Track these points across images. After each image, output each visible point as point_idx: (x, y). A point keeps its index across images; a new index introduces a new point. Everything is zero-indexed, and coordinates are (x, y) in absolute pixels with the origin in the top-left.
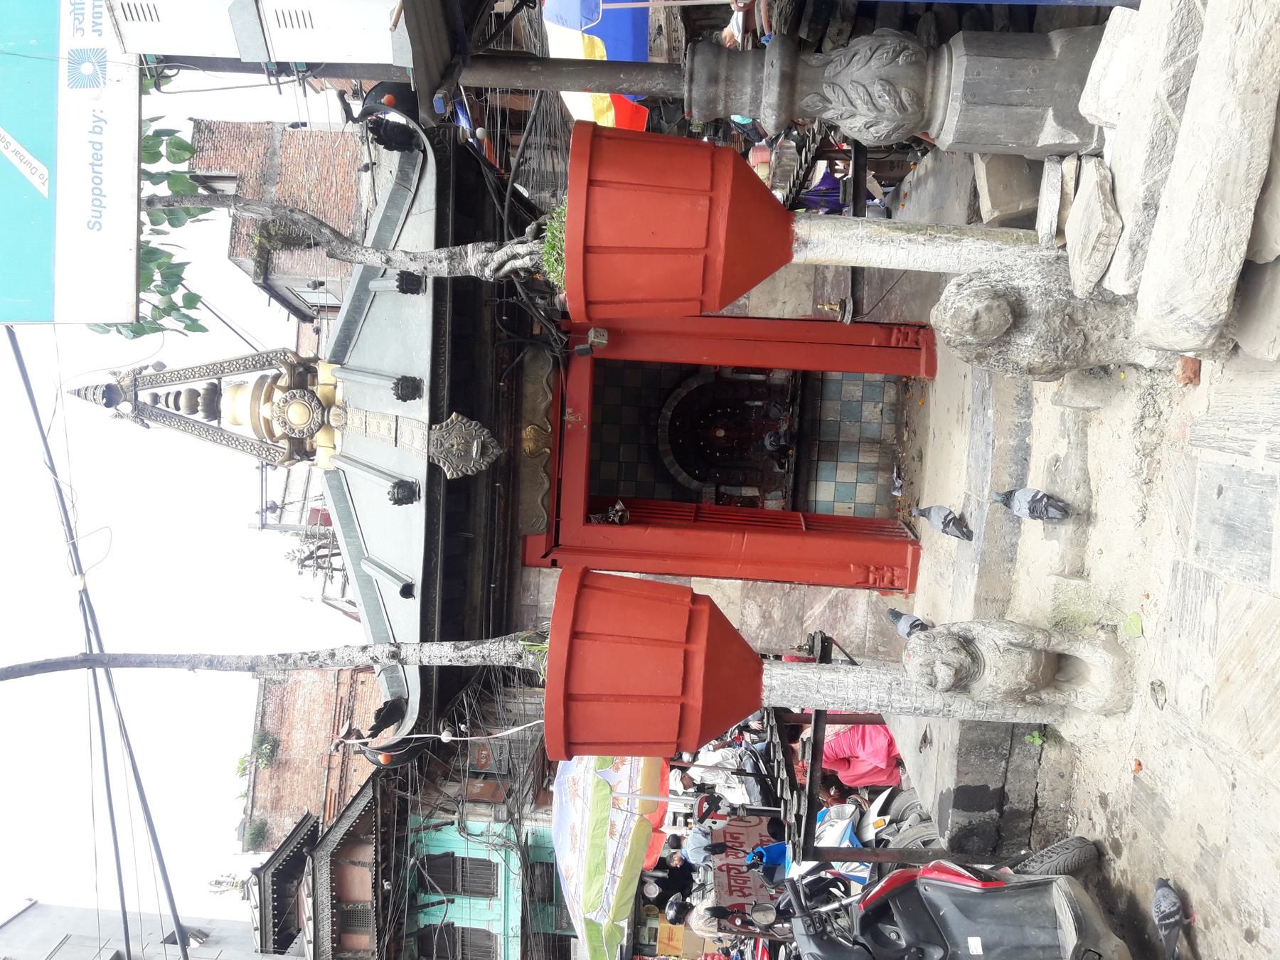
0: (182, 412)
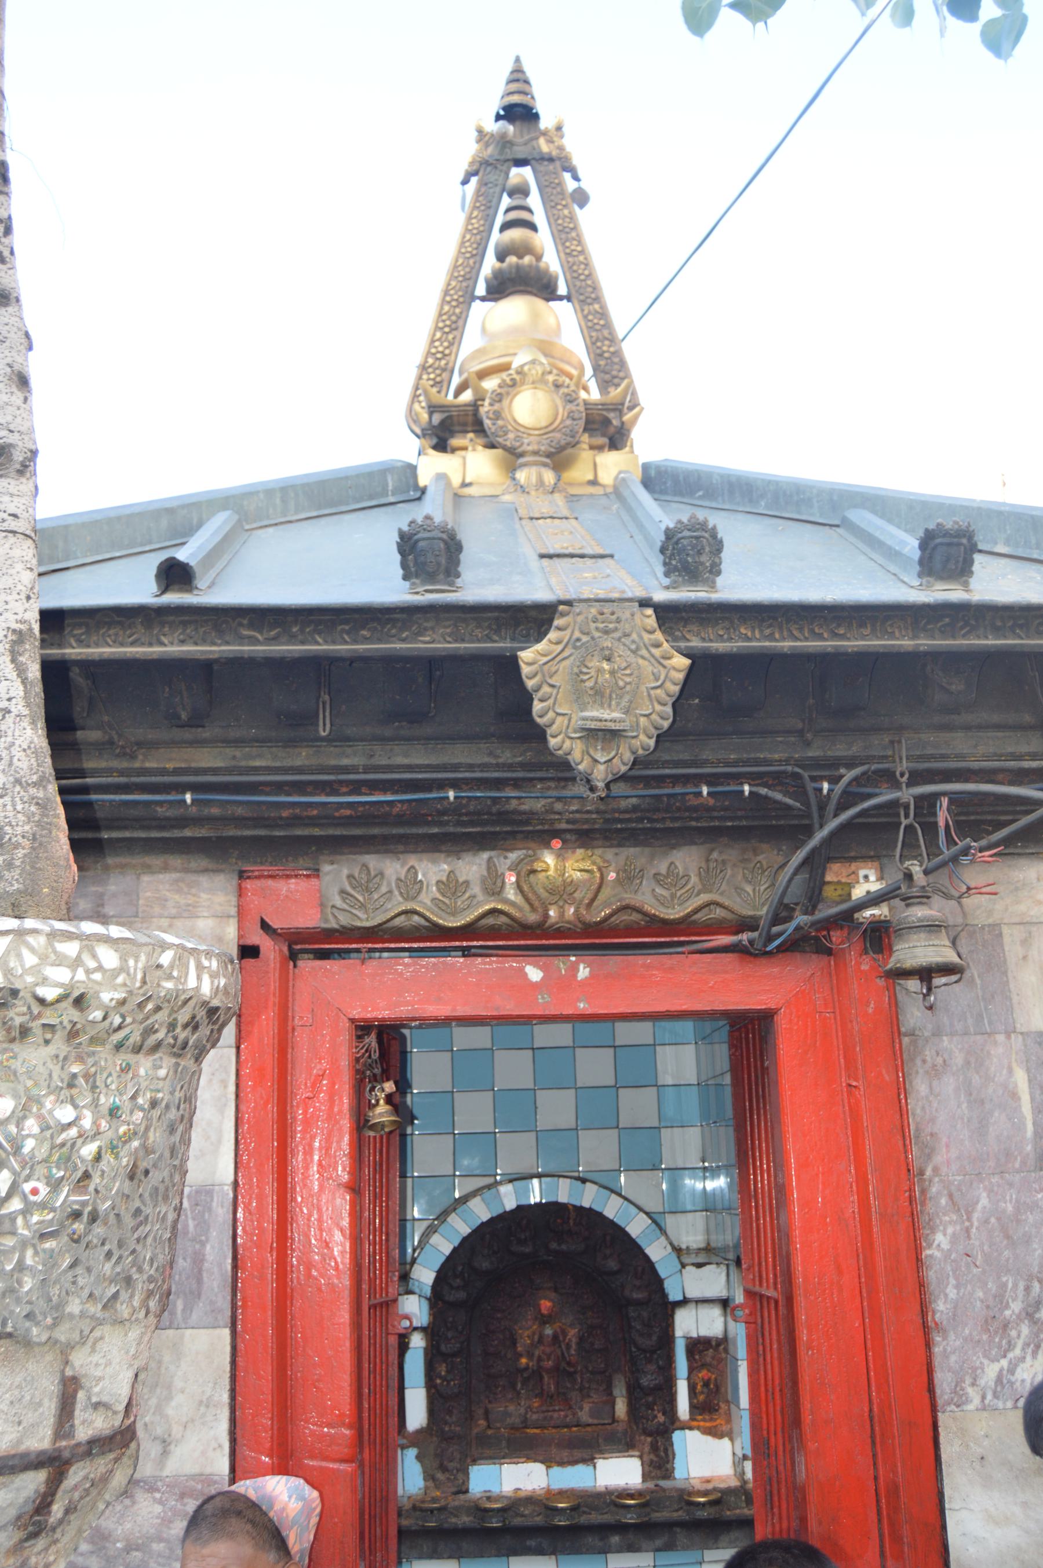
0: (495, 236)
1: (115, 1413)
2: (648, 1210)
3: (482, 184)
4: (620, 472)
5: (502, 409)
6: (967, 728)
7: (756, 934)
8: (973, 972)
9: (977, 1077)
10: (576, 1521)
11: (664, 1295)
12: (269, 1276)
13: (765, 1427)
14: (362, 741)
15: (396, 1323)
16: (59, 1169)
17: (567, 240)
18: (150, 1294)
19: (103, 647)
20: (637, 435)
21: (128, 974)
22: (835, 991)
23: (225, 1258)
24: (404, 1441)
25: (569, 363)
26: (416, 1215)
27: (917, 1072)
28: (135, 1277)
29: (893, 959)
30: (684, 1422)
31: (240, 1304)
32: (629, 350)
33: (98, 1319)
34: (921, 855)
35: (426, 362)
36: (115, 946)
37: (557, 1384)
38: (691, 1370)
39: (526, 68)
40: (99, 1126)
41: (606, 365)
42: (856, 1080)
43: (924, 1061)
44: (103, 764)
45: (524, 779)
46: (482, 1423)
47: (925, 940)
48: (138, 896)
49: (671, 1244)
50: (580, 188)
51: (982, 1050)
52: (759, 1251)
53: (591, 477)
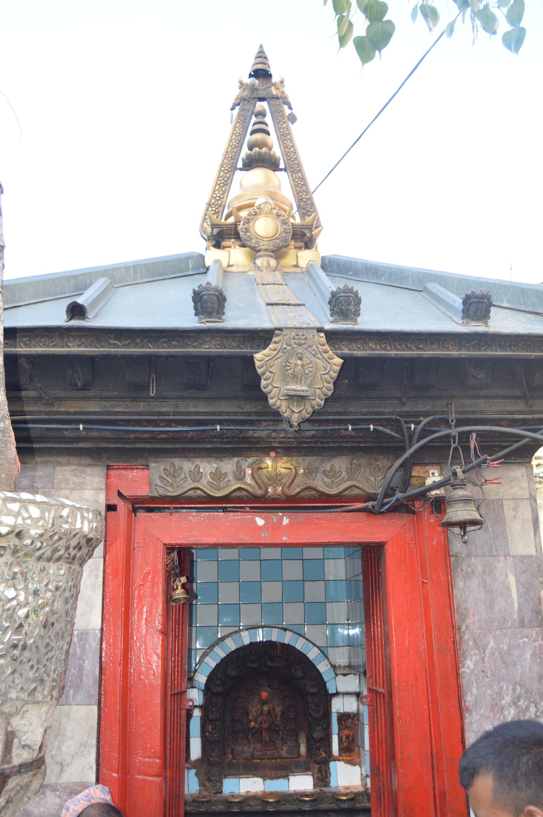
0: (248, 137)
1: (34, 750)
2: (318, 645)
3: (242, 110)
4: (310, 261)
5: (249, 227)
6: (486, 397)
7: (375, 503)
8: (488, 524)
9: (489, 579)
10: (278, 808)
11: (326, 690)
12: (119, 678)
13: (377, 760)
14: (172, 399)
15: (185, 704)
16: (6, 621)
17: (285, 140)
18: (53, 688)
19: (38, 347)
20: (319, 241)
21: (45, 521)
22: (416, 533)
23: (96, 668)
24: (189, 766)
25: (284, 204)
26: (198, 646)
27: (458, 576)
28: (46, 679)
29: (446, 517)
30: (336, 757)
31: (103, 693)
32: (317, 198)
33: (25, 701)
34: (461, 463)
35: (211, 201)
36: (38, 506)
37: (270, 738)
38: (340, 730)
39: (265, 51)
40: (28, 600)
41: (304, 205)
42: (426, 579)
43: (462, 570)
44: (37, 409)
45: (256, 420)
46: (230, 756)
47: (463, 507)
48: (54, 478)
49: (331, 664)
50: (292, 113)
51: (492, 564)
52: (376, 668)
53: (295, 263)
